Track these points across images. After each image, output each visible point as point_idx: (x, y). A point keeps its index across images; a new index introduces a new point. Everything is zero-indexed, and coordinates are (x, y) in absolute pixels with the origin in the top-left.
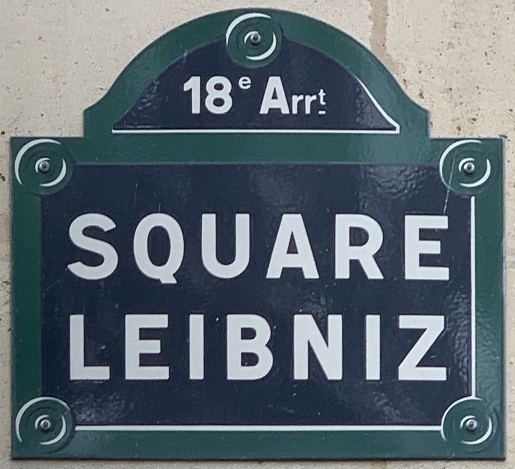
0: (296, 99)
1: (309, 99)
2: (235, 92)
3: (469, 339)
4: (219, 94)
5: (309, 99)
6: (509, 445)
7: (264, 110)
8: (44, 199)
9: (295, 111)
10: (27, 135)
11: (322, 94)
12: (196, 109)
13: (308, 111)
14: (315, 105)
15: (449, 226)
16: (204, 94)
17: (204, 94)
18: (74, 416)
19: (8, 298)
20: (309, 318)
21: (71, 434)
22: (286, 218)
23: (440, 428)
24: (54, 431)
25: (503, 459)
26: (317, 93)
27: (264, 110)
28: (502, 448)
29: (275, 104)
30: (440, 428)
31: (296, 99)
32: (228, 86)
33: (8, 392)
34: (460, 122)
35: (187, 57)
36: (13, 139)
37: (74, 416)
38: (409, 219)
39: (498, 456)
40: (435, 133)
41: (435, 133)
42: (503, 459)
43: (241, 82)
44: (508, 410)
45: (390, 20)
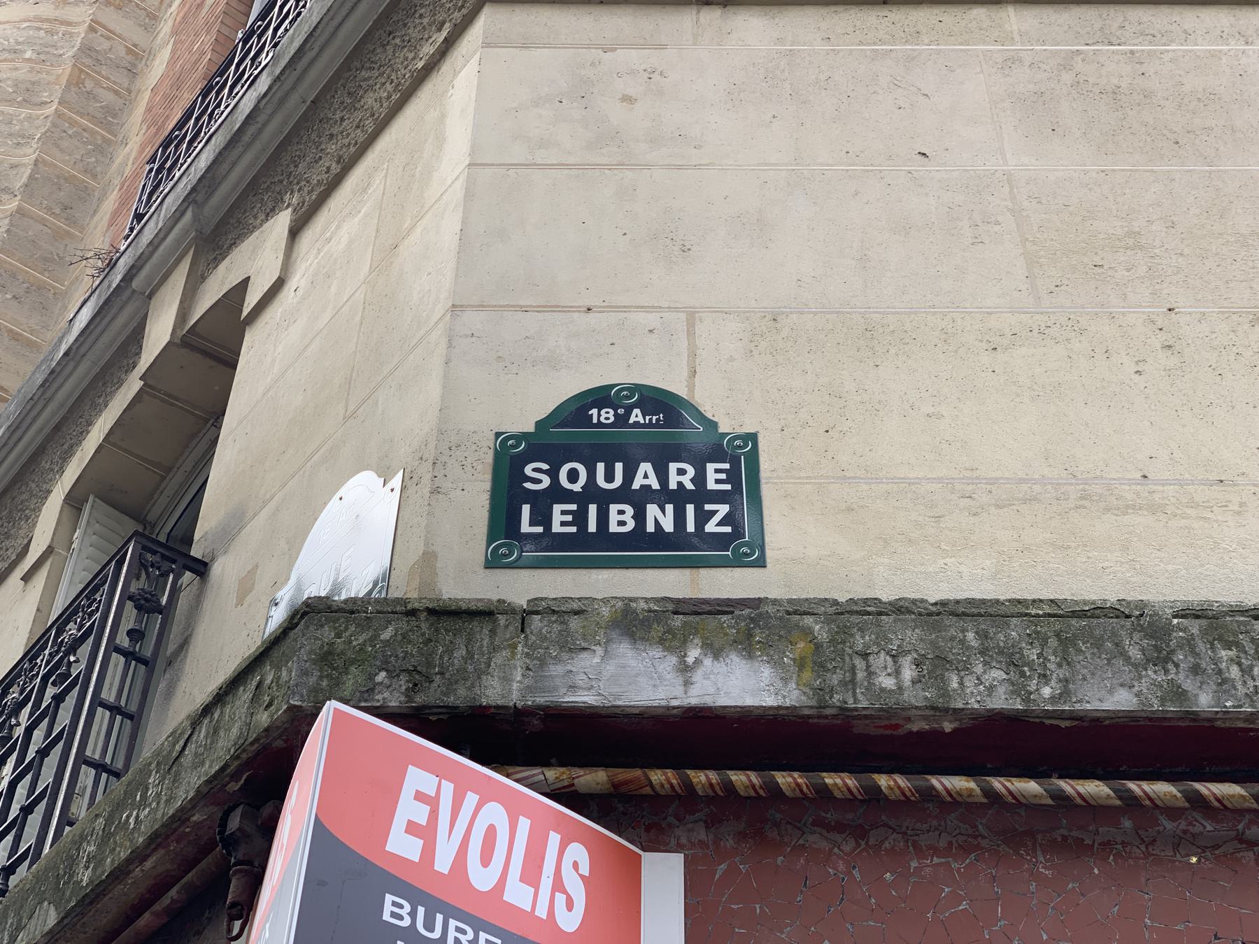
0: (647, 418)
1: (654, 418)
2: (616, 415)
3: (743, 515)
4: (607, 415)
5: (654, 418)
6: (768, 560)
7: (631, 421)
8: (511, 456)
9: (647, 422)
10: (504, 431)
11: (661, 415)
12: (595, 421)
13: (654, 422)
14: (658, 420)
15: (596, 465)
16: (599, 415)
17: (599, 415)
18: (522, 549)
19: (488, 497)
20: (655, 506)
21: (520, 556)
22: (366, 480)
23: (729, 553)
24: (511, 554)
25: (765, 567)
26: (659, 415)
27: (631, 421)
28: (765, 561)
29: (637, 419)
30: (729, 553)
31: (647, 418)
32: (612, 412)
33: (485, 538)
34: (735, 426)
35: (825, 784)
36: (496, 433)
37: (522, 549)
38: (708, 465)
39: (762, 565)
40: (721, 430)
41: (721, 430)
42: (765, 567)
43: (619, 411)
44: (766, 545)
45: (696, 388)
